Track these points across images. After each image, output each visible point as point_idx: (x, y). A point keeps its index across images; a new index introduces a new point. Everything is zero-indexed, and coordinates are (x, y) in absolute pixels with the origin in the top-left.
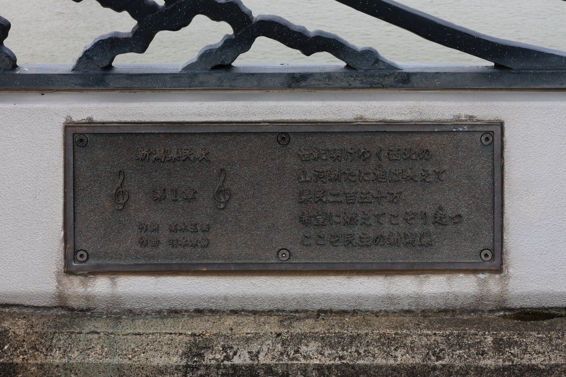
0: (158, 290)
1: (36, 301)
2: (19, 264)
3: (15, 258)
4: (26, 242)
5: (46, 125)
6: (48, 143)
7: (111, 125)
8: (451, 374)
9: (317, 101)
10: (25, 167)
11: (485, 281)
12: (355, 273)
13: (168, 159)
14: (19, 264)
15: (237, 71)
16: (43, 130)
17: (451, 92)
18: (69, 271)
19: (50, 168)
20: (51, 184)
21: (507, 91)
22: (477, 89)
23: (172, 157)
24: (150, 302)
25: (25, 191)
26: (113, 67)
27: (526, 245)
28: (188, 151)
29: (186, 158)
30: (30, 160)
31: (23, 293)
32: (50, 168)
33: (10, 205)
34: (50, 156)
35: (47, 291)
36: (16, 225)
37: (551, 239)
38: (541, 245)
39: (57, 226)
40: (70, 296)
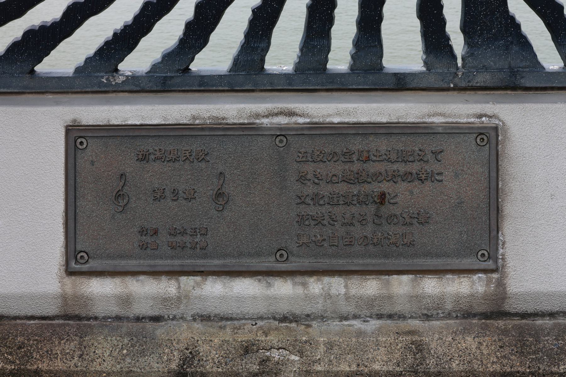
0: (23, 290)
1: (38, 301)
2: (21, 265)
3: (18, 259)
4: (28, 243)
5: (47, 127)
6: (49, 146)
7: (87, 128)
8: (494, 376)
9: (156, 104)
10: (27, 170)
11: (388, 282)
12: (457, 273)
13: (168, 159)
14: (21, 265)
15: (329, 72)
16: (44, 133)
17: (335, 94)
18: (70, 273)
19: (51, 170)
20: (52, 186)
21: (38, 95)
22: (188, 91)
23: (172, 158)
24: (15, 301)
25: (27, 193)
26: (35, 71)
27: (521, 245)
28: (187, 152)
29: (186, 159)
30: (32, 162)
31: (25, 294)
32: (51, 170)
33: (11, 207)
34: (52, 158)
35: (49, 291)
36: (17, 226)
37: (545, 239)
38: (536, 245)
39: (59, 228)
40: (208, 297)
